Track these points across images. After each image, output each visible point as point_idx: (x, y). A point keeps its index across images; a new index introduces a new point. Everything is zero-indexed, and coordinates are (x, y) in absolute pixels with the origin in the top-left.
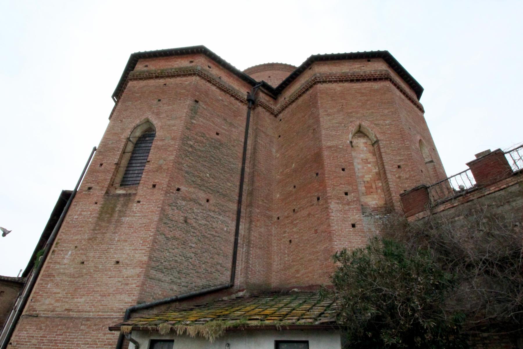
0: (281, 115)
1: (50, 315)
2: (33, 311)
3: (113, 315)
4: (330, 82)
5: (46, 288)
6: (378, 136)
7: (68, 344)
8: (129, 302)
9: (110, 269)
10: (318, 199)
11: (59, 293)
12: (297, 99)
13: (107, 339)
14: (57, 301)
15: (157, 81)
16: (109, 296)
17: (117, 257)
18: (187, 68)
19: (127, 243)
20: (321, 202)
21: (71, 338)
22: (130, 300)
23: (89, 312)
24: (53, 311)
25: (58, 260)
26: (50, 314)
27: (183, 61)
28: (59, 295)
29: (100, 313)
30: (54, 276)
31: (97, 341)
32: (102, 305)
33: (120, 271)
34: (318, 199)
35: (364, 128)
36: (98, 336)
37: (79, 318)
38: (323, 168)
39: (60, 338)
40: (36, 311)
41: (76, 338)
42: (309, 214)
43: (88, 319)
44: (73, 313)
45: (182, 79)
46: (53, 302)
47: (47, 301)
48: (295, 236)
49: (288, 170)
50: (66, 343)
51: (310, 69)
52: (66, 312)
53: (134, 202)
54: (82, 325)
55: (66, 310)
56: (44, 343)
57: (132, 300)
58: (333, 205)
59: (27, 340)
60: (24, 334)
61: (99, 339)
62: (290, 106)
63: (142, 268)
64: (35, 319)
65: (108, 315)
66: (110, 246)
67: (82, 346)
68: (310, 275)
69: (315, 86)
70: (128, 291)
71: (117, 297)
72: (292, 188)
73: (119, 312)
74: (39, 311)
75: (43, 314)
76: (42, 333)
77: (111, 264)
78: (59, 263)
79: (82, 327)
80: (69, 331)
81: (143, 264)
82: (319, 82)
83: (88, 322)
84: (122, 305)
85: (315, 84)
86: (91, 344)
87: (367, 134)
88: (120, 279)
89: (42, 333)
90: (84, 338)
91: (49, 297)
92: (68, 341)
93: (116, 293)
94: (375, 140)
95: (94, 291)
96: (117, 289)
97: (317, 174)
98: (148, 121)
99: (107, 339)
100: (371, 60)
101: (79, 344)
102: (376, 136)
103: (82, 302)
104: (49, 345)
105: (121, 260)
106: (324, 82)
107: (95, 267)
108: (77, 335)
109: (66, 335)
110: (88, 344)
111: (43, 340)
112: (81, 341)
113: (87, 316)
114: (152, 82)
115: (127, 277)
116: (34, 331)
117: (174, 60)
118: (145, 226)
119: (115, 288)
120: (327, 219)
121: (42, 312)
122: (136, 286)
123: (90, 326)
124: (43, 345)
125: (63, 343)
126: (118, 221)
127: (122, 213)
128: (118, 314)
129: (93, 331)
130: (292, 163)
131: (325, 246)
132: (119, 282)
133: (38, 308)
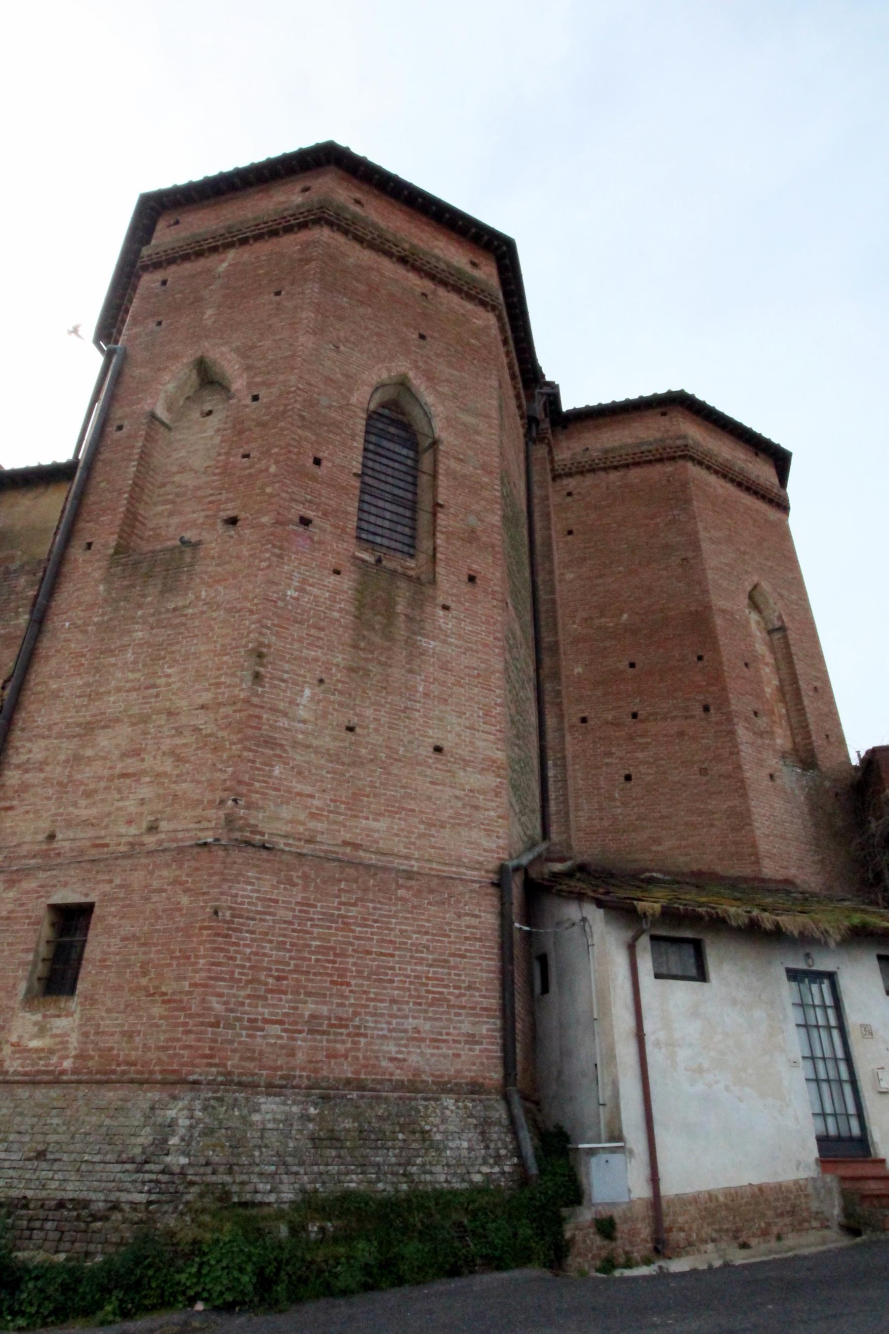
0: (571, 483)
1: (305, 851)
3: (465, 874)
4: (708, 468)
5: (270, 777)
6: (786, 619)
7: (378, 928)
8: (492, 851)
9: (426, 762)
10: (706, 709)
11: (312, 796)
13: (468, 927)
14: (312, 816)
16: (443, 827)
17: (435, 736)
18: (459, 271)
19: (448, 708)
20: (714, 716)
21: (381, 916)
22: (494, 846)
23: (407, 857)
24: (308, 841)
25: (281, 705)
26: (306, 849)
27: (453, 250)
28: (315, 802)
29: (434, 865)
30: (281, 746)
31: (447, 928)
32: (433, 847)
34: (706, 709)
35: (761, 594)
37: (385, 869)
38: (715, 648)
39: (354, 911)
40: (263, 834)
42: (681, 734)
43: (410, 875)
44: (368, 855)
46: (302, 817)
47: (286, 812)
48: (643, 769)
49: (608, 622)
50: (372, 927)
51: (664, 414)
52: (348, 850)
54: (399, 887)
55: (345, 843)
56: (312, 920)
57: (498, 847)
58: (742, 733)
59: (259, 908)
60: (245, 890)
62: (602, 474)
64: (264, 854)
66: (409, 703)
67: (415, 936)
68: (692, 852)
69: (681, 462)
70: (483, 824)
71: (463, 833)
72: (623, 665)
73: (476, 869)
74: (271, 834)
75: (286, 844)
77: (426, 751)
78: (285, 715)
79: (401, 892)
80: (371, 896)
81: (498, 768)
82: (692, 459)
83: (413, 883)
84: (479, 855)
85: (683, 457)
86: (434, 935)
87: (762, 606)
88: (457, 793)
91: (288, 803)
92: (376, 921)
93: (459, 825)
94: (777, 624)
95: (403, 809)
98: (403, 384)
99: (468, 927)
100: (761, 455)
101: (406, 931)
102: (780, 618)
103: (378, 829)
104: (330, 928)
105: (446, 745)
106: (700, 463)
108: (394, 908)
109: (368, 908)
110: (427, 933)
111: (307, 912)
112: (409, 925)
113: (405, 867)
115: (471, 791)
116: (274, 887)
117: (423, 226)
119: (451, 811)
120: (731, 753)
121: (282, 841)
122: (499, 817)
123: (420, 891)
124: (312, 926)
125: (366, 926)
126: (410, 643)
127: (416, 625)
128: (475, 873)
129: (429, 904)
130: (622, 612)
131: (731, 804)
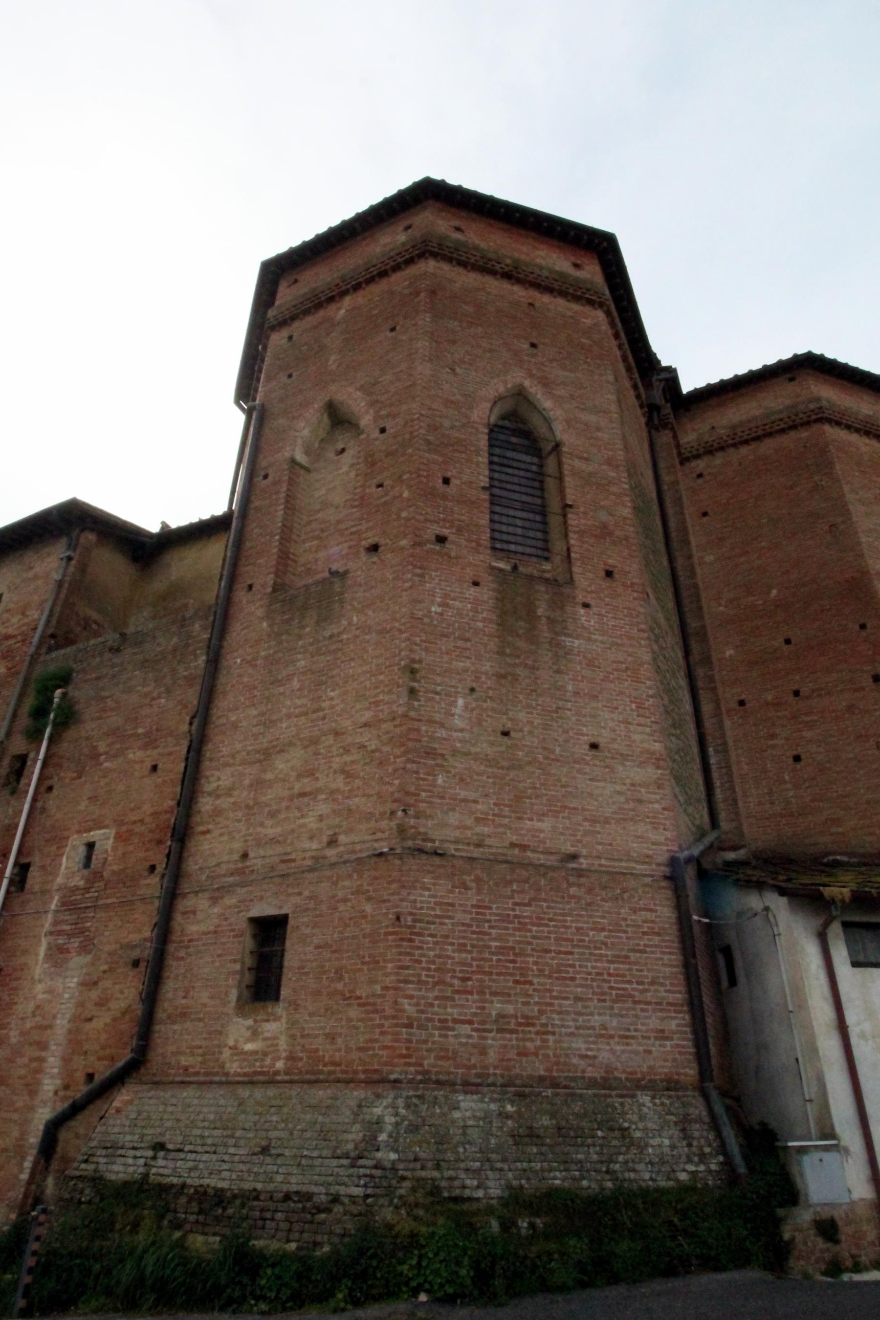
0: (700, 464)
1: (475, 855)
2: (424, 840)
3: (634, 868)
7: (555, 926)
12: (757, 439)
15: (506, 285)
25: (437, 717)
26: (476, 853)
29: (603, 862)
30: (442, 755)
33: (612, 770)
36: (619, 914)
40: (433, 841)
41: (570, 915)
42: (851, 708)
45: (567, 304)
46: (469, 822)
51: (792, 380)
53: (576, 603)
54: (570, 885)
55: (513, 845)
57: (666, 839)
61: (625, 919)
63: (658, 768)
65: (626, 868)
66: (561, 703)
67: (591, 933)
76: (472, 897)
78: (442, 725)
79: (573, 890)
80: (543, 896)
82: (829, 421)
85: (819, 420)
86: (610, 931)
89: (472, 897)
90: (591, 916)
96: (620, 809)
97: (863, 627)
98: (520, 394)
99: (644, 922)
101: (582, 928)
105: (602, 741)
107: (545, 748)
109: (541, 907)
114: (494, 285)
118: (627, 669)
128: (645, 867)
132: (619, 793)
133: (436, 834)
